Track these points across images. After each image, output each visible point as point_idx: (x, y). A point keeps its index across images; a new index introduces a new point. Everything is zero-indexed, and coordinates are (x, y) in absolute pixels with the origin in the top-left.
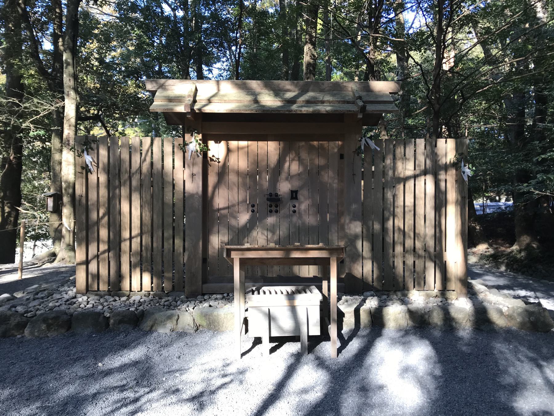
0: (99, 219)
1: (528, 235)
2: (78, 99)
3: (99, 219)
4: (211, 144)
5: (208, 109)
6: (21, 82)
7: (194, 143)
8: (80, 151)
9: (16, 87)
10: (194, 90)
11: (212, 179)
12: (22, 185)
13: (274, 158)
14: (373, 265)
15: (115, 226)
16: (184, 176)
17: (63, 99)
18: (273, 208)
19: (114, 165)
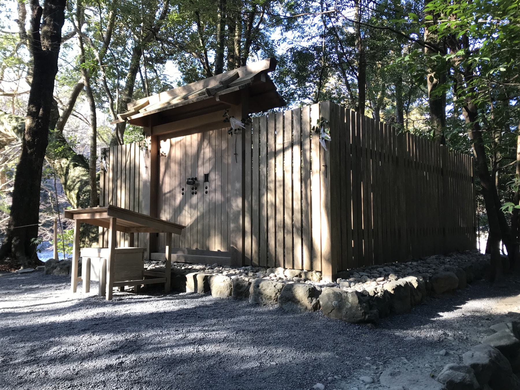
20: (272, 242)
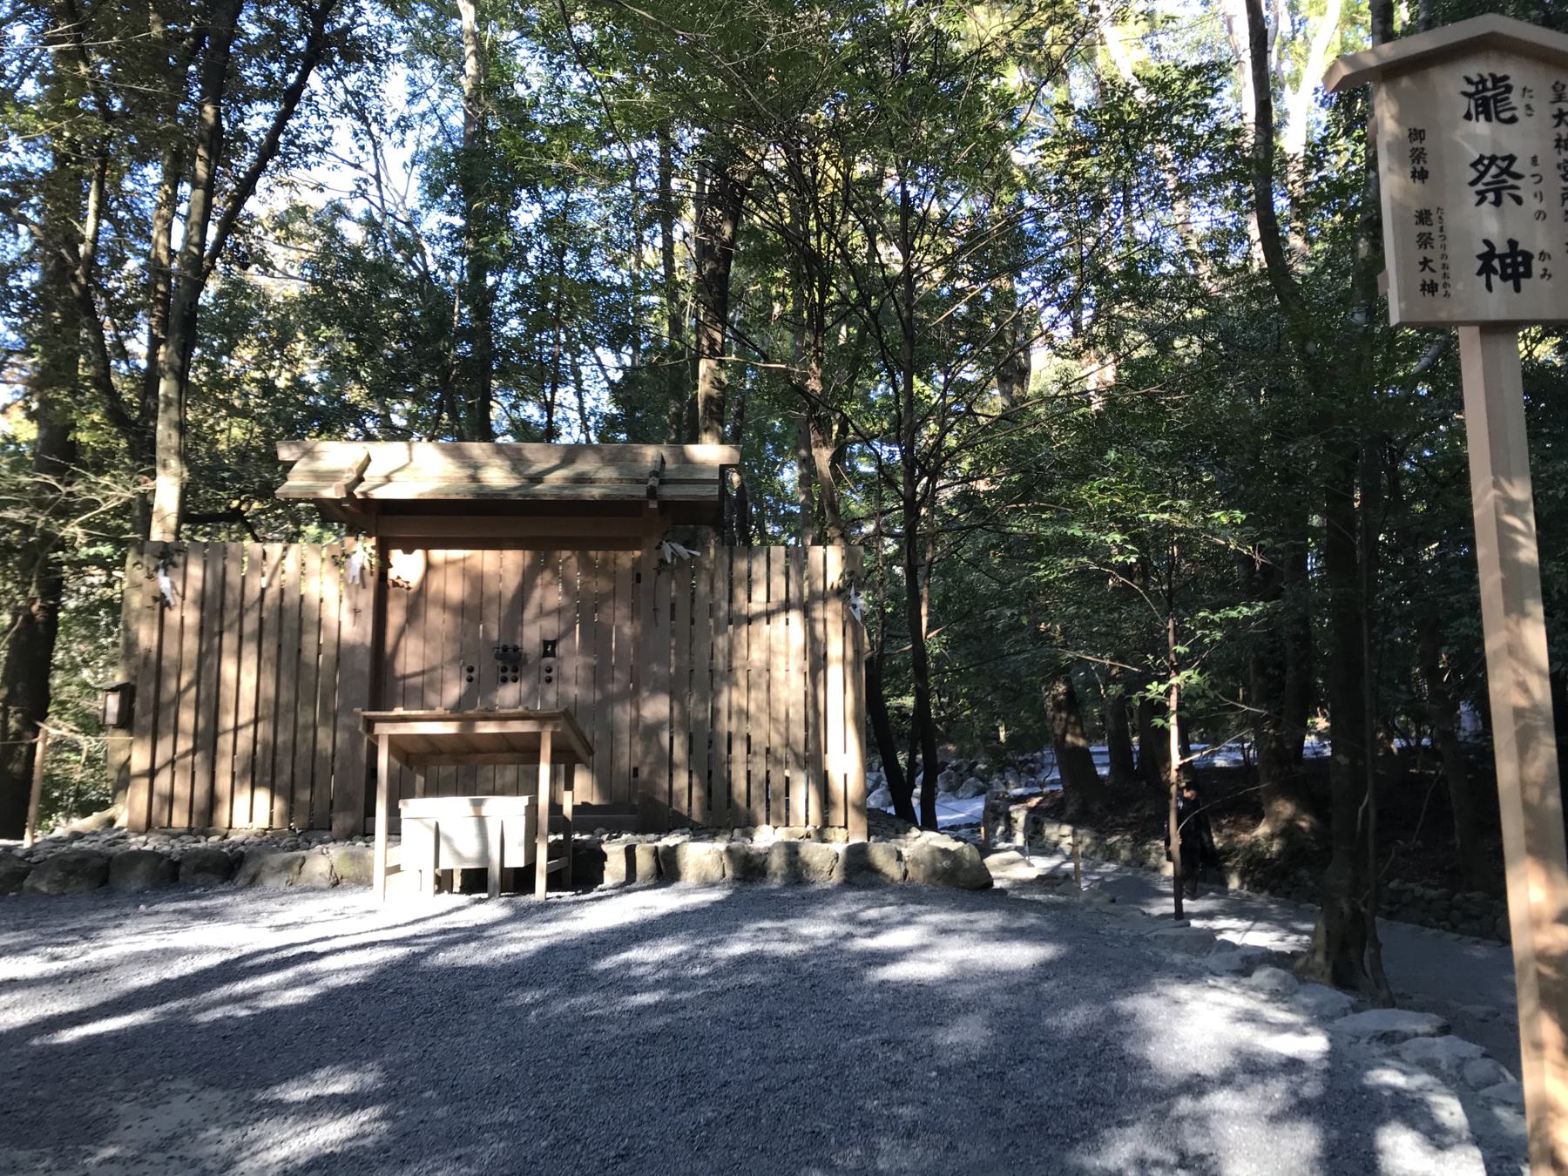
0: (180, 693)
1: (1288, 800)
2: (186, 474)
3: (179, 693)
4: (396, 555)
5: (378, 494)
6: (70, 438)
7: (362, 551)
8: (152, 567)
9: (58, 452)
10: (362, 458)
11: (395, 617)
12: (57, 680)
13: (512, 582)
14: (690, 777)
15: (210, 705)
16: (340, 612)
17: (152, 475)
18: (509, 674)
19: (214, 593)
20: (740, 785)
